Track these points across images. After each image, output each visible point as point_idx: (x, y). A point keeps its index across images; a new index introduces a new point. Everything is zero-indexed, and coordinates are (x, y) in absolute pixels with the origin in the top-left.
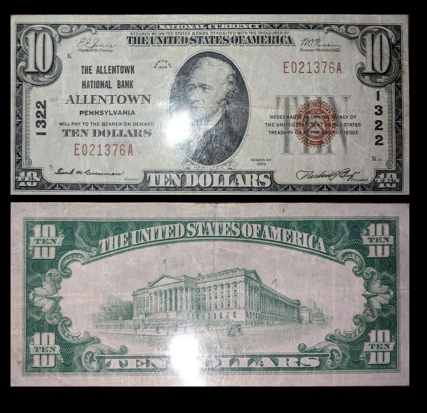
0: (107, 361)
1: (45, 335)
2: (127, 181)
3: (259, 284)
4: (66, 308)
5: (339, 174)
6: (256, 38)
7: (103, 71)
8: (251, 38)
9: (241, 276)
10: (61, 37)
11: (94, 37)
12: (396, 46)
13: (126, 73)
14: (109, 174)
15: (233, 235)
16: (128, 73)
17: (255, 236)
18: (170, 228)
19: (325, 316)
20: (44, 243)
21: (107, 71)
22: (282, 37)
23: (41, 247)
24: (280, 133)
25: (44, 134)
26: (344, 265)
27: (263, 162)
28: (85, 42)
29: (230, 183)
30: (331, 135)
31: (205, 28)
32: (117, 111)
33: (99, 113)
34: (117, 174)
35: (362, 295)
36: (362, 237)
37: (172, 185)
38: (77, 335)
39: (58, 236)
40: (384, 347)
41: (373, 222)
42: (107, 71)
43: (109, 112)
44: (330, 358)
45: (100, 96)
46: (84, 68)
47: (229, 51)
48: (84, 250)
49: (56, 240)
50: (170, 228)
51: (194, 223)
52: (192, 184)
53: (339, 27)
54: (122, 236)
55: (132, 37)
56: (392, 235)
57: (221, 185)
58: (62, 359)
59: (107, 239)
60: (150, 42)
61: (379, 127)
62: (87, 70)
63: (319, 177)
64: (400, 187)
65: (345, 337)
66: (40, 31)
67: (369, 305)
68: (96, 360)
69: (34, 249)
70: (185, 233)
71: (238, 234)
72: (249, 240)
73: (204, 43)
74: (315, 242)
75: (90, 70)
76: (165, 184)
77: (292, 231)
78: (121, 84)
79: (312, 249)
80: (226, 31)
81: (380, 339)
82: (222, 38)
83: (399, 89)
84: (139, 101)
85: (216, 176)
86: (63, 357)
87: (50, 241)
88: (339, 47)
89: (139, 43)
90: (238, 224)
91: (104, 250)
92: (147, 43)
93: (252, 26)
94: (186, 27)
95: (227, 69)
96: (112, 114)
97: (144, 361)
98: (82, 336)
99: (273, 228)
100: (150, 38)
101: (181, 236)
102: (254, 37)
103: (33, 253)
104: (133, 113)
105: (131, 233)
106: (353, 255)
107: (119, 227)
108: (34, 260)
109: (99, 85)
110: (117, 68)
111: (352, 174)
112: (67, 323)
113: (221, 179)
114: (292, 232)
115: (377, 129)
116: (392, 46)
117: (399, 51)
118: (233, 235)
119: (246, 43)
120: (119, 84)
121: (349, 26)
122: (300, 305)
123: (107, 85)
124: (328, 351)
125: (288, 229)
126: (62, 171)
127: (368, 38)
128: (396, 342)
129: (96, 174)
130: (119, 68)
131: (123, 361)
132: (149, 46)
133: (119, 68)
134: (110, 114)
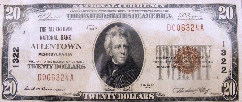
7: (53, 30)
8: (145, 15)
13: (66, 31)
21: (55, 30)
25: (18, 66)
28: (43, 15)
31: (116, 7)
32: (61, 53)
33: (50, 54)
34: (61, 90)
42: (55, 30)
45: (51, 45)
60: (81, 17)
61: (224, 62)
62: (43, 29)
63: (187, 92)
73: (115, 18)
78: (63, 38)
82: (127, 14)
84: (75, 47)
88: (202, 18)
100: (81, 15)
104: (71, 54)
109: (50, 38)
110: (61, 28)
113: (133, 95)
115: (223, 63)
119: (142, 18)
123: (55, 38)
126: (28, 88)
130: (63, 28)
132: (81, 19)
133: (63, 28)
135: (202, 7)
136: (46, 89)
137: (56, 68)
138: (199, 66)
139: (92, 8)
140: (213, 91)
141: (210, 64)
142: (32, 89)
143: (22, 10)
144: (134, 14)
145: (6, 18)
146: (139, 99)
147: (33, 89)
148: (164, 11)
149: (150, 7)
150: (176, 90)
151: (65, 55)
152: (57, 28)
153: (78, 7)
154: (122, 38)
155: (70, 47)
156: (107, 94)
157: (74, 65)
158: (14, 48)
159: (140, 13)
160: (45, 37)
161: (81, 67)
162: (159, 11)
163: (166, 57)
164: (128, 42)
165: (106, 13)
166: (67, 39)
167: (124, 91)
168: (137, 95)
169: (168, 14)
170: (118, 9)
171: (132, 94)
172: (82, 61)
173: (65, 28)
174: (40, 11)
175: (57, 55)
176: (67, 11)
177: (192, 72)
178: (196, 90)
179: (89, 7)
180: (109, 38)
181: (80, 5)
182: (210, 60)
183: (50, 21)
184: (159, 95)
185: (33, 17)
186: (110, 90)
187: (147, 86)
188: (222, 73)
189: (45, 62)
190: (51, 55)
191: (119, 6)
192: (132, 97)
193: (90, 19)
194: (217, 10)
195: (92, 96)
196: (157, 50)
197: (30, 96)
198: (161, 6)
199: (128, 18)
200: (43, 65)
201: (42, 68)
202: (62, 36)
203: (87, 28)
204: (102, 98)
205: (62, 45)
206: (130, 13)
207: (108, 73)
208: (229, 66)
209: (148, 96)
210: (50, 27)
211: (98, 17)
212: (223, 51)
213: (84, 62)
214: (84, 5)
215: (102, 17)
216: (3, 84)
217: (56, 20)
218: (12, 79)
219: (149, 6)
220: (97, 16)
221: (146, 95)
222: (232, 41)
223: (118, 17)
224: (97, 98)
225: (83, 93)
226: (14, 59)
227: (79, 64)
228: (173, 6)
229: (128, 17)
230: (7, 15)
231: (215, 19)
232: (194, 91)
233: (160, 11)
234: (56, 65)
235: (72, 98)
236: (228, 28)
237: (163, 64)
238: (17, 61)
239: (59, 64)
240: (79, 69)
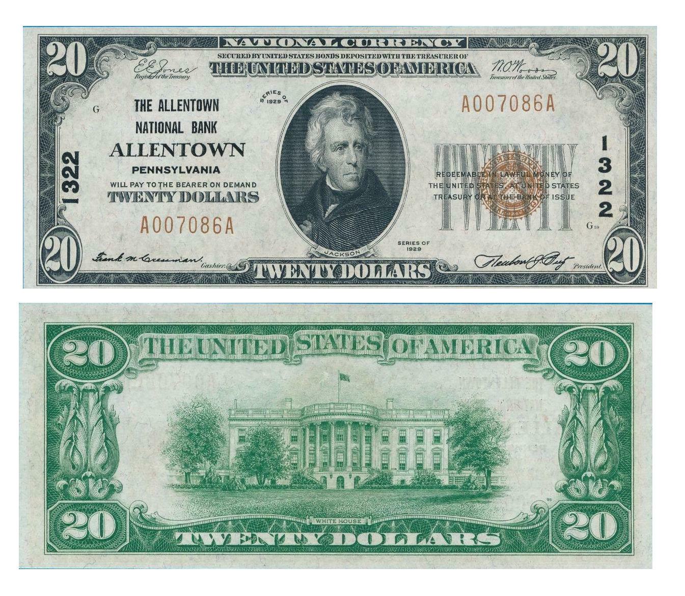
5: (542, 259)
7: (169, 107)
8: (409, 65)
13: (205, 110)
14: (195, 260)
16: (210, 110)
21: (175, 107)
25: (76, 201)
28: (146, 65)
29: (387, 275)
30: (536, 201)
31: (336, 44)
32: (191, 167)
33: (164, 170)
34: (191, 261)
42: (175, 107)
45: (165, 146)
63: (510, 264)
73: (334, 73)
75: (149, 105)
78: (198, 127)
82: (364, 65)
96: (184, 173)
104: (217, 170)
110: (191, 103)
111: (563, 261)
113: (378, 269)
115: (602, 192)
119: (402, 73)
123: (176, 128)
126: (104, 257)
129: (158, 260)
130: (195, 103)
132: (245, 76)
133: (195, 103)
134: (181, 172)
135: (555, 46)
136: (153, 260)
137: (184, 201)
138: (544, 197)
139: (261, 47)
140: (579, 260)
141: (572, 191)
143: (90, 51)
144: (381, 64)
145: (48, 72)
146: (393, 277)
147: (119, 259)
148: (456, 56)
149: (422, 45)
150: (482, 261)
152: (182, 103)
153: (309, 44)
154: (351, 125)
155: (214, 152)
156: (313, 265)
157: (229, 194)
158: (67, 154)
159: (395, 60)
160: (149, 125)
161: (247, 197)
162: (442, 56)
163: (462, 174)
164: (366, 137)
165: (311, 62)
167: (355, 257)
168: (388, 267)
169: (467, 64)
170: (339, 52)
171: (376, 265)
172: (251, 184)
173: (201, 103)
174: (140, 55)
175: (182, 171)
176: (212, 54)
177: (526, 213)
179: (267, 44)
180: (318, 125)
181: (314, 40)
182: (572, 180)
184: (442, 268)
185: (122, 71)
186: (322, 255)
187: (413, 246)
189: (154, 185)
190: (165, 172)
191: (344, 43)
192: (376, 273)
193: (268, 76)
194: (593, 51)
195: (274, 270)
196: (437, 153)
197: (114, 273)
198: (450, 44)
199: (366, 73)
200: (148, 193)
202: (193, 123)
203: (263, 98)
204: (301, 277)
206: (371, 60)
207: (316, 216)
208: (619, 200)
209: (416, 271)
211: (290, 72)
212: (602, 162)
213: (254, 185)
214: (255, 40)
215: (301, 72)
216: (42, 242)
218: (67, 231)
219: (420, 43)
220: (287, 68)
221: (410, 269)
222: (632, 132)
224: (288, 276)
225: (251, 262)
226: (67, 182)
227: (242, 189)
228: (479, 42)
229: (366, 70)
230: (50, 63)
231: (586, 77)
232: (529, 262)
233: (446, 56)
234: (184, 192)
235: (226, 278)
236: (622, 99)
237: (453, 191)
238: (74, 187)
239: (192, 190)
240: (242, 203)
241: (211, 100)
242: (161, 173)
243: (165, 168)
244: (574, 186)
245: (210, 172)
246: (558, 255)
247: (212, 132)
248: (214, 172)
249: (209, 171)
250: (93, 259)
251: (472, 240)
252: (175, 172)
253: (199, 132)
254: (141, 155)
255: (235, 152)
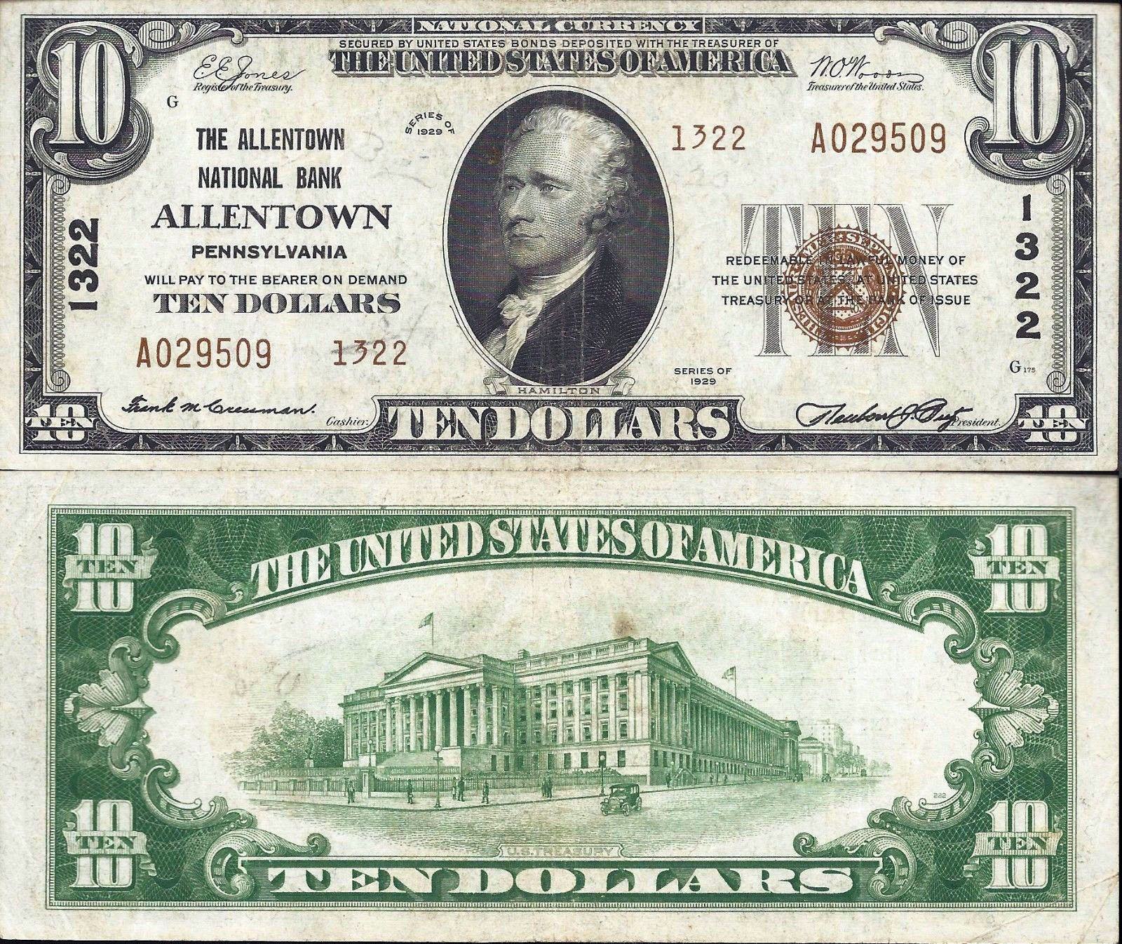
0: (273, 873)
1: (105, 807)
2: (332, 427)
3: (688, 680)
4: (164, 739)
5: (915, 412)
6: (687, 56)
7: (257, 142)
8: (673, 55)
9: (641, 657)
10: (150, 54)
11: (239, 51)
12: (1080, 74)
13: (321, 148)
14: (274, 410)
15: (615, 552)
17: (677, 554)
18: (444, 533)
19: (869, 763)
20: (102, 570)
21: (268, 142)
22: (759, 54)
23: (95, 581)
24: (755, 300)
25: (93, 306)
26: (922, 631)
27: (708, 377)
28: (215, 66)
31: (548, 28)
32: (296, 247)
33: (247, 252)
34: (295, 411)
35: (971, 709)
36: (972, 558)
37: (457, 436)
38: (194, 806)
39: (141, 554)
40: (1030, 845)
41: (1002, 520)
42: (268, 142)
43: (273, 250)
44: (879, 872)
46: (205, 134)
47: (616, 90)
48: (210, 588)
49: (134, 562)
50: (444, 533)
51: (509, 521)
52: (513, 433)
53: (919, 26)
54: (313, 553)
55: (345, 53)
56: (1054, 555)
57: (594, 435)
58: (152, 867)
59: (272, 561)
63: (858, 421)
64: (1085, 443)
65: (924, 818)
66: (91, 38)
67: (986, 736)
68: (244, 870)
69: (76, 586)
70: (485, 546)
71: (630, 548)
72: (663, 565)
73: (543, 69)
74: (841, 572)
76: (439, 434)
77: (779, 542)
78: (307, 177)
79: (832, 591)
80: (606, 38)
81: (1020, 825)
82: (595, 56)
83: (1085, 186)
85: (579, 415)
86: (153, 862)
87: (118, 566)
88: (917, 78)
89: (363, 68)
90: (632, 522)
91: (263, 590)
92: (385, 69)
93: (677, 26)
94: (494, 26)
95: (607, 140)
96: (284, 257)
97: (373, 872)
98: (205, 807)
99: (726, 535)
101: (474, 553)
102: (682, 54)
103: (75, 595)
104: (341, 252)
105: (338, 547)
106: (946, 607)
107: (304, 529)
108: (76, 613)
110: (295, 134)
112: (164, 776)
113: (593, 419)
114: (777, 546)
115: (1021, 294)
116: (1066, 75)
117: (1088, 86)
118: (615, 552)
119: (660, 69)
120: (303, 177)
121: (947, 21)
122: (800, 733)
123: (270, 179)
124: (875, 854)
125: (767, 536)
126: (142, 404)
127: (1001, 53)
128: (1065, 833)
130: (303, 135)
131: (317, 873)
132: (391, 75)
133: (303, 135)
134: (277, 256)
136: (229, 410)
142: (163, 409)
147: (168, 408)
150: (808, 414)
151: (315, 257)
155: (336, 223)
158: (76, 224)
160: (222, 173)
166: (325, 171)
175: (280, 254)
178: (902, 415)
183: (246, 92)
188: (1018, 336)
190: (249, 256)
201: (207, 311)
202: (299, 169)
205: (301, 211)
210: (243, 131)
211: (465, 68)
212: (1023, 241)
215: (485, 67)
217: (275, 88)
223: (554, 67)
224: (429, 433)
232: (892, 416)
238: (89, 280)
241: (331, 130)
242: (244, 257)
243: (250, 249)
244: (970, 281)
245: (330, 256)
246: (943, 405)
247: (333, 187)
248: (335, 257)
249: (326, 256)
250: (123, 408)
251: (786, 379)
252: (267, 257)
253: (309, 186)
254: (207, 224)
255: (374, 220)
